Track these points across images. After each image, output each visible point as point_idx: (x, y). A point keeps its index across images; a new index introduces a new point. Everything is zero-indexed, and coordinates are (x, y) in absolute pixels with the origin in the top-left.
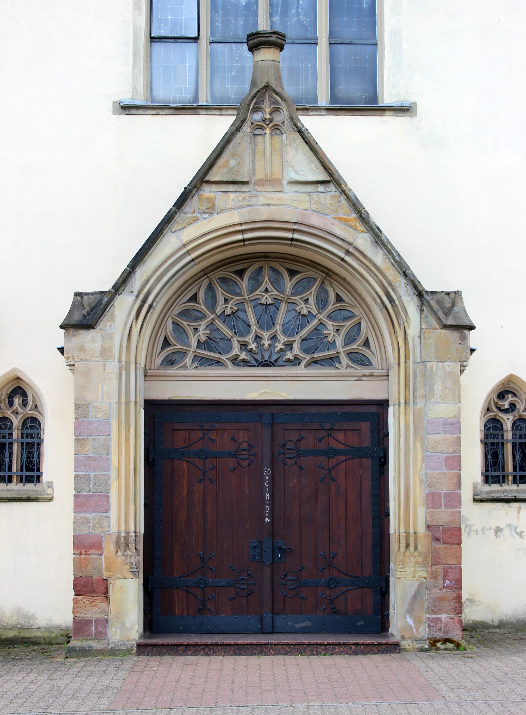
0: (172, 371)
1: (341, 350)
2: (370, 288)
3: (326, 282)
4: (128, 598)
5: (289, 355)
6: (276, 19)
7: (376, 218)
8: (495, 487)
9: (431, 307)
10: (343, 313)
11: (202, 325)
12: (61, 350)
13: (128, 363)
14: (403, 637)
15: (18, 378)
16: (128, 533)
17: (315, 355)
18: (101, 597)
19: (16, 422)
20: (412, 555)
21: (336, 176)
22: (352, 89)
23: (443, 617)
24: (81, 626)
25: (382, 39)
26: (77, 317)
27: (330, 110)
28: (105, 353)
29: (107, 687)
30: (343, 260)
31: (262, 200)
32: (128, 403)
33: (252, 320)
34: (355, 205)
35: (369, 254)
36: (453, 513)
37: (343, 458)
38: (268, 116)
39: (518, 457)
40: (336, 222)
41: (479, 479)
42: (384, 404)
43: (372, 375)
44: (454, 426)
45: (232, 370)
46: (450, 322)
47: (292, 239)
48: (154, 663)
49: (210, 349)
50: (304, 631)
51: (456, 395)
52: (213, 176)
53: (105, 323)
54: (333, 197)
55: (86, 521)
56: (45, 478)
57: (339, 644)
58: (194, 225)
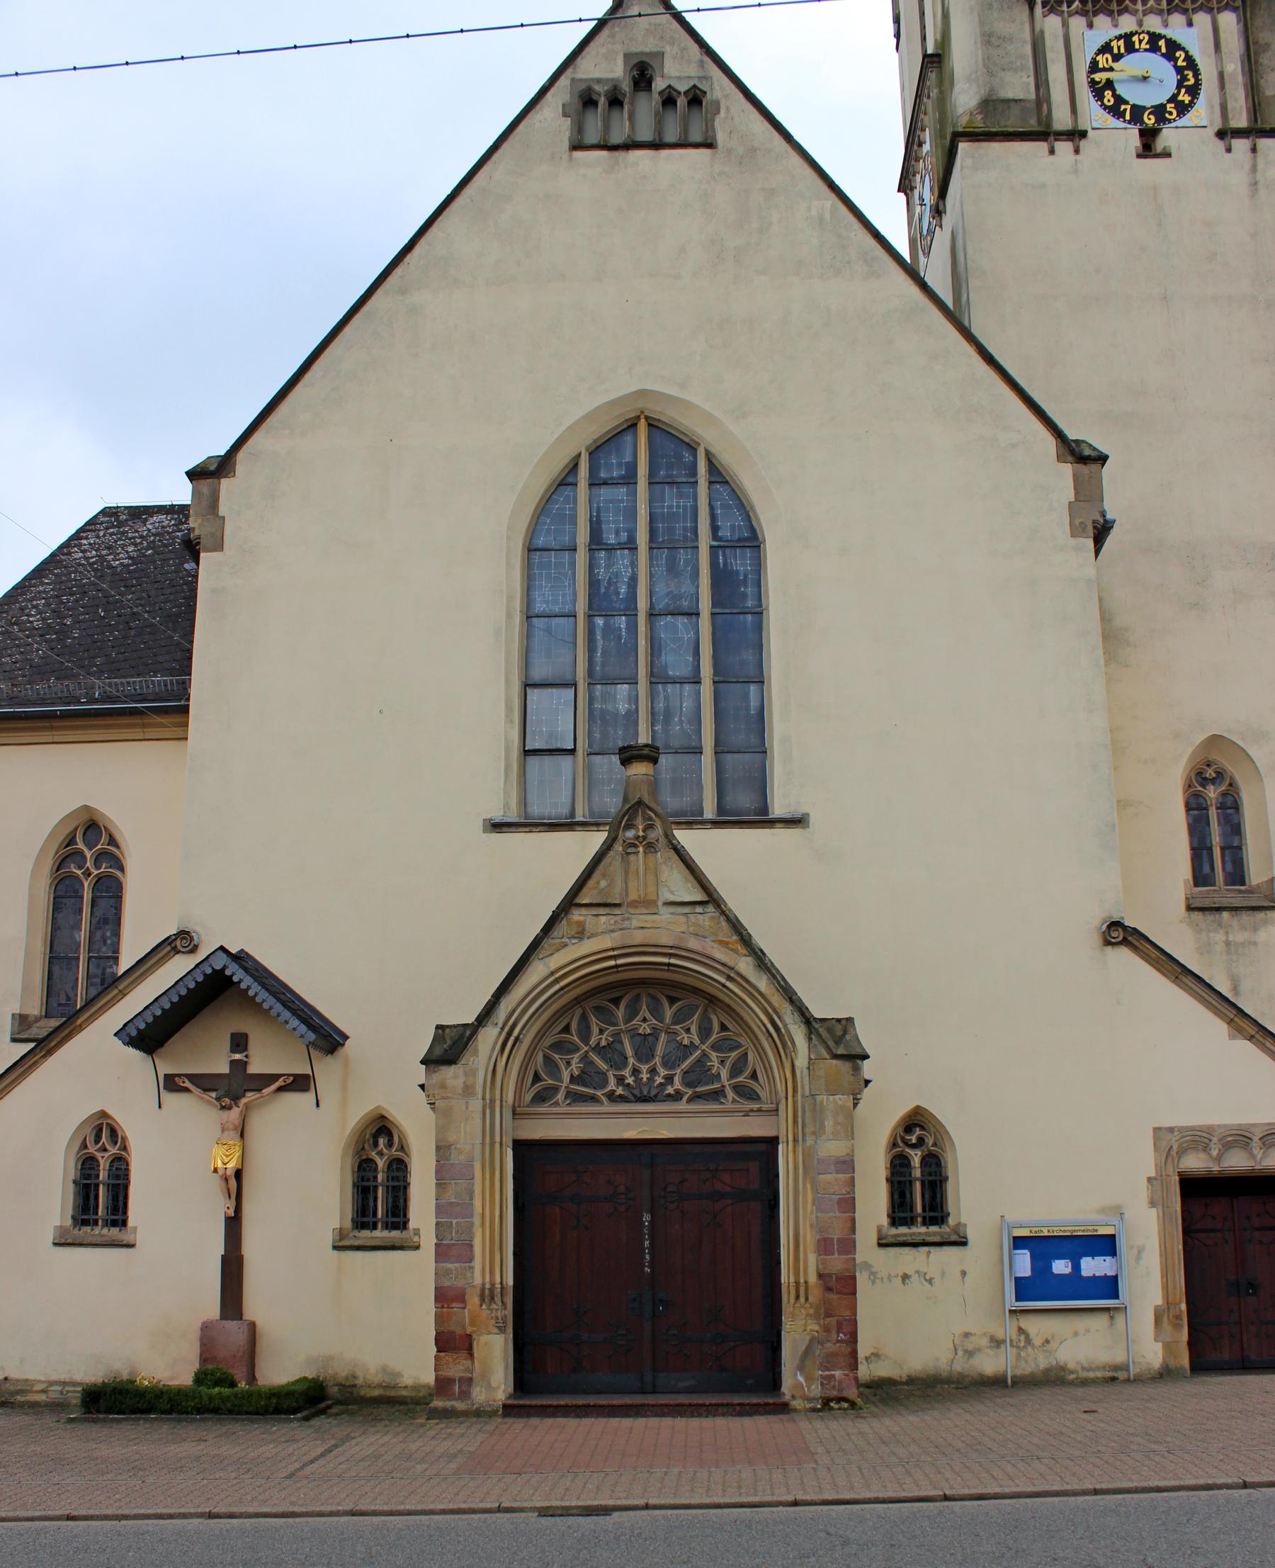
0: (542, 1109)
1: (726, 1084)
2: (756, 1016)
3: (710, 1010)
4: (495, 1357)
5: (670, 1090)
6: (658, 728)
7: (760, 940)
8: (903, 1230)
9: (819, 1036)
10: (728, 1042)
11: (575, 1058)
12: (422, 1087)
13: (492, 1101)
14: (793, 1397)
15: (383, 1117)
16: (493, 1284)
17: (698, 1089)
18: (464, 1354)
19: (381, 1163)
20: (802, 1306)
21: (715, 896)
22: (743, 800)
23: (838, 1373)
24: (443, 1385)
25: (772, 746)
26: (438, 1052)
27: (716, 824)
28: (468, 1090)
29: (461, 1451)
30: (724, 985)
31: (635, 923)
32: (492, 1144)
33: (629, 1051)
34: (736, 927)
35: (752, 979)
36: (848, 1260)
37: (729, 1202)
38: (641, 834)
39: (927, 1196)
40: (716, 945)
41: (884, 1221)
42: (773, 1142)
43: (759, 1110)
44: (847, 1164)
45: (608, 1107)
46: (840, 1051)
47: (669, 965)
48: (517, 1425)
49: (585, 1085)
50: (688, 1391)
51: (849, 1129)
52: (584, 898)
53: (467, 1059)
54: (712, 918)
55: (448, 1272)
56: (412, 1225)
57: (723, 1405)
58: (563, 951)
